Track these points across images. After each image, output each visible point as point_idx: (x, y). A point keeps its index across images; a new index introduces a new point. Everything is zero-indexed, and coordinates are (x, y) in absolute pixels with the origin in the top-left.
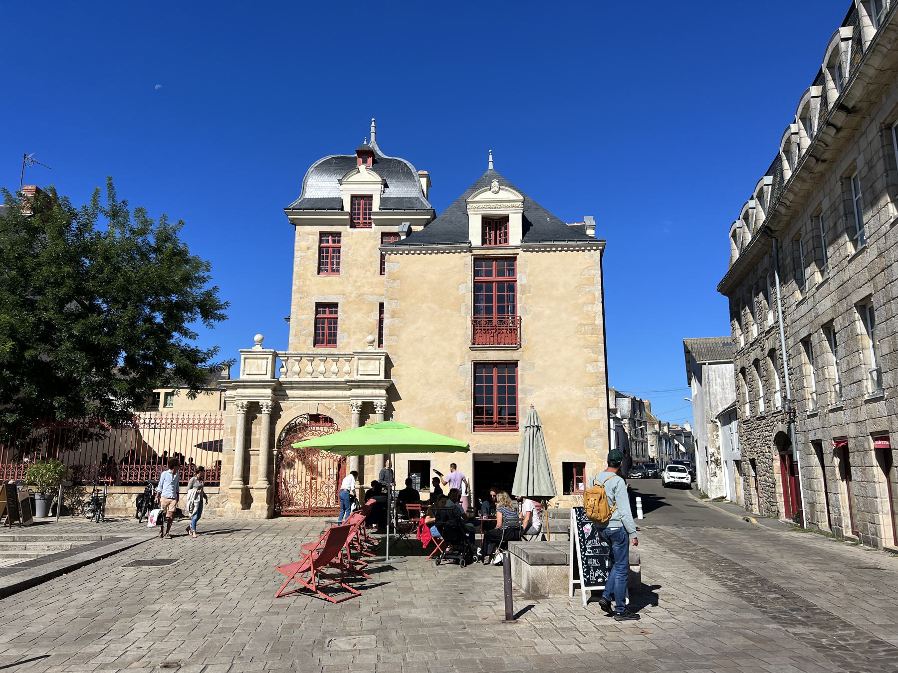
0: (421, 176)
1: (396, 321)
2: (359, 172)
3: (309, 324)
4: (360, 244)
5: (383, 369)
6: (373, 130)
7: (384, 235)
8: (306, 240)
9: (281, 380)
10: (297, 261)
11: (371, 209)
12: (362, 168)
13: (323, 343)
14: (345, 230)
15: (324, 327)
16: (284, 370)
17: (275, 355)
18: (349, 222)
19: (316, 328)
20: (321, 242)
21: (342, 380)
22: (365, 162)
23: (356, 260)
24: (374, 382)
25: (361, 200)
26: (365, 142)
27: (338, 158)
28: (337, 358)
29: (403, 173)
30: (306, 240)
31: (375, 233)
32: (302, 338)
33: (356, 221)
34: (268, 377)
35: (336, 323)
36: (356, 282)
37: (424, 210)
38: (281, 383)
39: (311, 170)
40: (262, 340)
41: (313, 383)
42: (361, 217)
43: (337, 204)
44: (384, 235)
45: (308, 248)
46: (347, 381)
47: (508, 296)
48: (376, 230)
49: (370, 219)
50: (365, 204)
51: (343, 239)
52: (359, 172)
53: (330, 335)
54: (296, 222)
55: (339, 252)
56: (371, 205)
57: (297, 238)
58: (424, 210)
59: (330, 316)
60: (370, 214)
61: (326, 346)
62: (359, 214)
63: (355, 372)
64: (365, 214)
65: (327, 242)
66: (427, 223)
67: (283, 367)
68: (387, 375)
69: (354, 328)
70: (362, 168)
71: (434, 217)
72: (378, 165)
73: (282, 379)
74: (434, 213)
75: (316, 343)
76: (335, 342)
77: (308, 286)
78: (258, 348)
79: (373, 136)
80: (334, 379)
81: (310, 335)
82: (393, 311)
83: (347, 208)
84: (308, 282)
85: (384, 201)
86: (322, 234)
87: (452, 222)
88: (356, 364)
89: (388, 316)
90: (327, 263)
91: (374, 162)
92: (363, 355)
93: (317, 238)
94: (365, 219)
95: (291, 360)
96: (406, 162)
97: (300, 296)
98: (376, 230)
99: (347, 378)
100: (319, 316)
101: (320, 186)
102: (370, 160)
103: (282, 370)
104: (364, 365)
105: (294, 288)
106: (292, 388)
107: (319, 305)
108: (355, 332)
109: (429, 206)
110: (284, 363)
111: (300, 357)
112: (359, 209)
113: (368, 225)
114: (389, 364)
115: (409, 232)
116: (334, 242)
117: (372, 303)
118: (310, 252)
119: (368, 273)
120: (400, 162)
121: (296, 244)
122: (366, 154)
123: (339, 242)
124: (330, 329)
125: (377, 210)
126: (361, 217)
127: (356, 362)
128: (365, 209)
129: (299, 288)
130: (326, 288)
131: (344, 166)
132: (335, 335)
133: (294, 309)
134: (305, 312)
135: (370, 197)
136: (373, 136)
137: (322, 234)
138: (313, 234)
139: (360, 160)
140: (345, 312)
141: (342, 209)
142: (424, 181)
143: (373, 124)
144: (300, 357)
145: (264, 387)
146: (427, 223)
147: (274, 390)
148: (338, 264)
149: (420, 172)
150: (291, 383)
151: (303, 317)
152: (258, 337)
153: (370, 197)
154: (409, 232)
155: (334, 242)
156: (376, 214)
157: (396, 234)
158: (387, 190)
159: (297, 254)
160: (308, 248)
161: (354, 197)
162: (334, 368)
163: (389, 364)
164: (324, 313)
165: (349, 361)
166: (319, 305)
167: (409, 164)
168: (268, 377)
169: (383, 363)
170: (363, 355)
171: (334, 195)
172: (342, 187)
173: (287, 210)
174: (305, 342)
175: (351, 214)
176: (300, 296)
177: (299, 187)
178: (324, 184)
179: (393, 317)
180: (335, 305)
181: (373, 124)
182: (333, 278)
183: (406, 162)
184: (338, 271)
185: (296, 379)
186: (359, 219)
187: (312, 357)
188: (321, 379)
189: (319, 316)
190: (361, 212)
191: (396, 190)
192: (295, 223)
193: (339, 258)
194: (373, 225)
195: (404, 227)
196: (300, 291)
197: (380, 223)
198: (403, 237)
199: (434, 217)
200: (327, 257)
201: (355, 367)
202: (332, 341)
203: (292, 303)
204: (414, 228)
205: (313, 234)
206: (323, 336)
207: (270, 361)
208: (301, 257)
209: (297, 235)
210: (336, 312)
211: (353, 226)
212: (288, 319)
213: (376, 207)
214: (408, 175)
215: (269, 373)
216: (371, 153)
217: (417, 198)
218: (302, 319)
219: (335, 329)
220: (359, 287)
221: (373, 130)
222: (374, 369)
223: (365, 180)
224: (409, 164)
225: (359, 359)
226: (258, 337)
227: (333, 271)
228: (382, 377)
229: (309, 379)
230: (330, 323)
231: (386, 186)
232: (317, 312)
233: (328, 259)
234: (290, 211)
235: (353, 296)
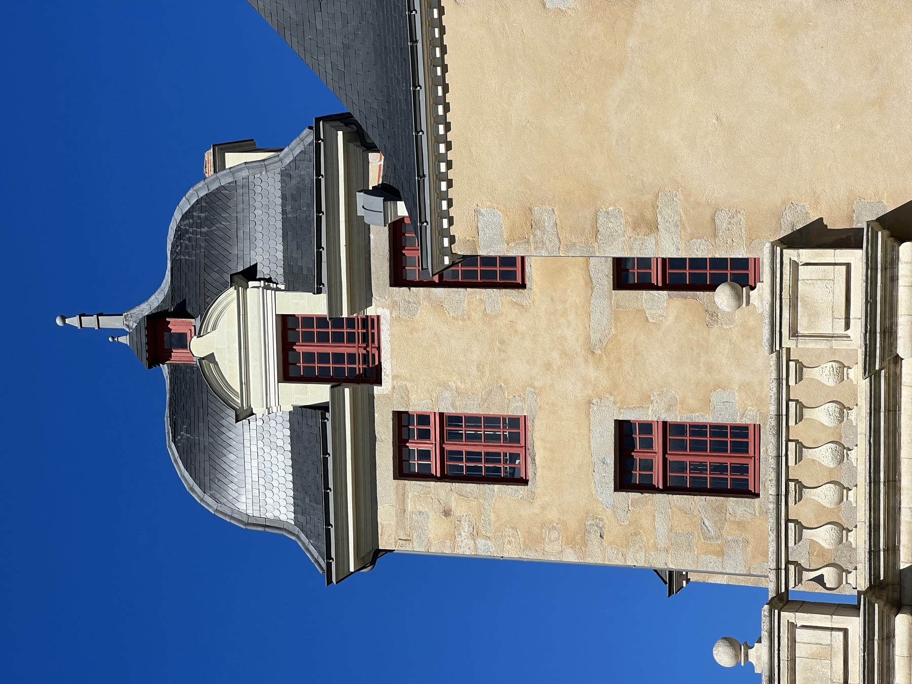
0: (219, 165)
1: (665, 216)
2: (211, 358)
3: (684, 511)
4: (430, 349)
5: (829, 255)
6: (89, 322)
7: (398, 279)
8: (421, 519)
9: (863, 585)
10: (485, 548)
11: (321, 321)
12: (199, 347)
13: (744, 469)
14: (387, 397)
15: (696, 467)
16: (829, 575)
17: (783, 601)
18: (360, 387)
19: (698, 489)
20: (424, 475)
21: (863, 385)
22: (182, 341)
23: (480, 367)
24: (870, 282)
25: (297, 350)
26: (124, 340)
27: (174, 425)
28: (789, 408)
29: (210, 221)
30: (421, 519)
31: (394, 305)
32: (730, 532)
33: (359, 367)
34: (855, 625)
35: (679, 428)
36: (548, 366)
37: (320, 152)
38: (876, 586)
39: (210, 504)
40: (732, 642)
41: (874, 481)
42: (345, 349)
43: (308, 425)
44: (398, 279)
45: (447, 513)
46: (870, 371)
47: (693, 434)
48: (386, 305)
49: (351, 322)
50: (308, 338)
51: (417, 405)
52: (211, 358)
53: (719, 447)
54: (367, 549)
55: (455, 420)
56: (308, 320)
57: (417, 547)
58: (320, 152)
59: (658, 445)
60: (338, 322)
61: (756, 459)
62: (338, 358)
63: (836, 344)
64: (338, 338)
65: (424, 455)
66: (361, 142)
67: (820, 580)
68: (848, 239)
69: (696, 359)
70: (199, 347)
71: (345, 120)
72: (190, 303)
73: (859, 580)
74: (327, 119)
75: (744, 490)
76: (741, 431)
77: (563, 512)
78: (759, 655)
79: (108, 322)
80: (860, 417)
81: (721, 510)
82: (636, 226)
83: (319, 393)
84: (553, 515)
85: (297, 279)
86: (402, 472)
87: (346, 47)
88: (811, 345)
89: (650, 242)
90: (492, 457)
91: (181, 312)
92: (782, 325)
93: (413, 487)
94: (351, 338)
95: (799, 554)
96: (177, 216)
97: (594, 537)
98: (386, 305)
99: (856, 373)
100: (658, 481)
101: (259, 481)
102: (176, 325)
103: (830, 581)
104: (814, 315)
105: (570, 557)
106: (893, 549)
107: (624, 481)
108: (710, 368)
109: (307, 136)
110: (808, 575)
111: (787, 526)
112: (324, 357)
113: (369, 329)
114: (814, 236)
115: (387, 192)
116: (424, 435)
117: (616, 315)
118: (460, 509)
119: (521, 327)
120: (180, 234)
121: (434, 550)
122: (159, 339)
123: (424, 419)
124: (698, 447)
125: (323, 298)
126: (345, 349)
127: (804, 344)
128: (323, 338)
129: (571, 542)
130: (570, 459)
131: (199, 406)
132: (719, 430)
133: (636, 559)
134: (646, 522)
135: (287, 325)
136: (108, 322)
137: (402, 472)
138: (402, 499)
139: (177, 355)
140: (646, 399)
141: (322, 408)
142: (233, 159)
143: (73, 321)
144: (787, 526)
145: (888, 638)
146: (361, 142)
147: (898, 606)
148: (492, 421)
149: (209, 170)
150: (873, 553)
151: (662, 529)
152: (723, 656)
153: (287, 325)
154: (387, 192)
155: (424, 435)
156: (334, 302)
157: (397, 230)
158: (263, 271)
159: (465, 547)
160: (447, 513)
161: (288, 374)
162: (825, 495)
163: (814, 236)
164: (648, 465)
165: (800, 367)
166: (624, 481)
167: (184, 205)
168: (855, 625)
169: (805, 255)
170: (782, 325)
171: (282, 435)
172: (258, 409)
173: (332, 575)
174: (741, 525)
175: (336, 380)
176: (594, 537)
177: (262, 537)
178: (252, 465)
179: (653, 227)
180: (623, 429)
181: (73, 321)
182: (540, 439)
183: (177, 216)
184: (514, 422)
185: (859, 538)
186: (352, 358)
187: (790, 488)
188: (859, 456)
189: (658, 481)
190: (330, 349)
191: (265, 247)
192: (372, 555)
193: (474, 420)
194: (370, 311)
195: (370, 207)
196: (580, 540)
197: (362, 292)
198: (402, 209)
199: (345, 120)
200: (473, 456)
201: (822, 345)
202: (738, 438)
203: (618, 561)
204: (375, 179)
205: (402, 499)
206: (721, 468)
207: (801, 618)
208: (475, 534)
209: (408, 548)
210: (646, 427)
211: (374, 376)
212: (672, 580)
213: (312, 304)
214: (214, 205)
215: (840, 621)
216: (156, 324)
217: (286, 175)
218: (666, 533)
219: (699, 429)
220: (564, 354)
221: (89, 322)
222: (828, 284)
223: (234, 338)
224: (184, 205)
225: (794, 333)
226: (723, 656)
227: (515, 438)
228: (856, 257)
229: (859, 497)
230: (681, 446)
231: (250, 273)
232: (647, 487)
233: (481, 451)
234: (330, 558)
235: (592, 373)
